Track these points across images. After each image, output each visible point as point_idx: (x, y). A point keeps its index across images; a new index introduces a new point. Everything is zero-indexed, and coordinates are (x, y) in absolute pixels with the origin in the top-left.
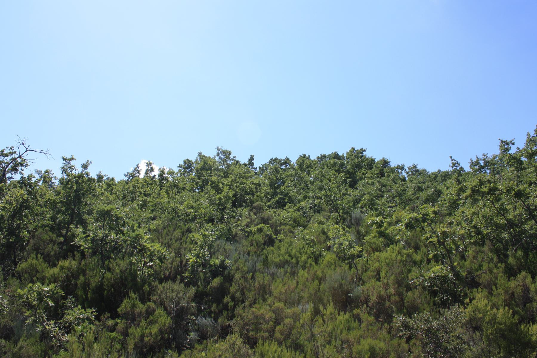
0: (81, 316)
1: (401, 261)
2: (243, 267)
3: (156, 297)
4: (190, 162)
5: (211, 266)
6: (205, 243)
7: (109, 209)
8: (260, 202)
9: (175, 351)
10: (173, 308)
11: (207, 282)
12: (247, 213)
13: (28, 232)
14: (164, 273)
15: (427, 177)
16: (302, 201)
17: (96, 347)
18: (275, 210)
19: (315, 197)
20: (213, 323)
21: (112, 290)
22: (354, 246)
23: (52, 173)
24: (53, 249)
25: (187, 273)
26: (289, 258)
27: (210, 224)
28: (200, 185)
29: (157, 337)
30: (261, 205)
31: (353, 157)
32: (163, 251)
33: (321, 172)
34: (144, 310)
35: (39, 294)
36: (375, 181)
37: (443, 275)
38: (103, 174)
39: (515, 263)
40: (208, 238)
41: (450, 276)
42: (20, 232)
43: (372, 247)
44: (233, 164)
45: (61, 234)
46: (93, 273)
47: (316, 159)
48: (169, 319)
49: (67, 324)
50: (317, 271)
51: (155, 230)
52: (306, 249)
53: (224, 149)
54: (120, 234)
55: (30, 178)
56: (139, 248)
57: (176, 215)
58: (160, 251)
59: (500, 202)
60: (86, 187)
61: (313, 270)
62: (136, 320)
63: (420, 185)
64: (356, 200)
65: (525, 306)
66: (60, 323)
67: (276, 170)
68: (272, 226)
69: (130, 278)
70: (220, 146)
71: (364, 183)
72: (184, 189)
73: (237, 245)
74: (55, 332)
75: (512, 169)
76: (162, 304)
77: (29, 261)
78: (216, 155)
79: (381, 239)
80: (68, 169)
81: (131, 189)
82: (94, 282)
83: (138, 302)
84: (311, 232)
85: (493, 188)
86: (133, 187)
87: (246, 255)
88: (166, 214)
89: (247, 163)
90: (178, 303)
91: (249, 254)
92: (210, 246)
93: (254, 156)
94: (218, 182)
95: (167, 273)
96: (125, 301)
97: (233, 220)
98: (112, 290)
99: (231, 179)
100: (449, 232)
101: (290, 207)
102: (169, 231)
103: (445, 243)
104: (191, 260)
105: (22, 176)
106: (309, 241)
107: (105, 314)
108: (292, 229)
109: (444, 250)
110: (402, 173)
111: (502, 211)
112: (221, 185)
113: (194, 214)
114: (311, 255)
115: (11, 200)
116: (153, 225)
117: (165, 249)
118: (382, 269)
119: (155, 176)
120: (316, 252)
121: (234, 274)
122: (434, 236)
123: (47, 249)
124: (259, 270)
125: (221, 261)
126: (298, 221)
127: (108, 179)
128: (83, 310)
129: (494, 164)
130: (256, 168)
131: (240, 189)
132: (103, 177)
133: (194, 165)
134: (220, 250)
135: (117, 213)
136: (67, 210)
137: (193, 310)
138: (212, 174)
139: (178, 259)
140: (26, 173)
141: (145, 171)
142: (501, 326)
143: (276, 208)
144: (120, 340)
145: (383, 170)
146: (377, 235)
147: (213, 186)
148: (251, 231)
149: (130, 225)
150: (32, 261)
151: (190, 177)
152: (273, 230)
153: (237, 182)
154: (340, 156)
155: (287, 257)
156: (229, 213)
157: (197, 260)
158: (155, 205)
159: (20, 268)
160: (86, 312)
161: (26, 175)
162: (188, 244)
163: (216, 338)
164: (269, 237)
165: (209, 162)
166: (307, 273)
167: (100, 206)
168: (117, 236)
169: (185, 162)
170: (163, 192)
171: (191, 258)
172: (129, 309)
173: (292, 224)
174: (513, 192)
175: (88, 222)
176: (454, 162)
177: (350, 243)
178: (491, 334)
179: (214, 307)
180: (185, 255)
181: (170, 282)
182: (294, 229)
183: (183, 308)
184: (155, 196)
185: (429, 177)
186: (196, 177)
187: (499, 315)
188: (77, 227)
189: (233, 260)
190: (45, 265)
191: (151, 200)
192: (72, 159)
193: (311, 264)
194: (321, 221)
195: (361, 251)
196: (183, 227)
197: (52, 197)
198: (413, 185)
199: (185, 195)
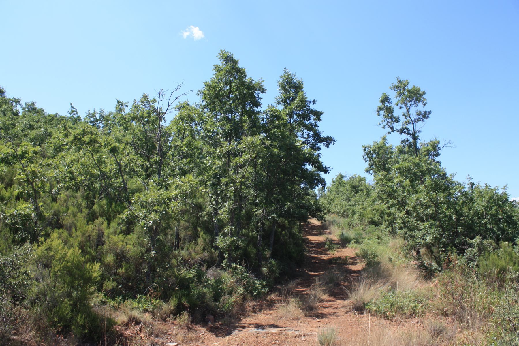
15: (44, 117)
37: (26, 213)
39: (98, 210)
41: (33, 215)
59: (99, 154)
63: (32, 123)
65: (97, 247)
75: (121, 128)
85: (93, 139)
100: (39, 172)
103: (34, 183)
109: (31, 189)
110: (16, 106)
111: (100, 163)
122: (23, 173)
129: (108, 120)
142: (69, 264)
174: (110, 147)
176: (73, 110)
178: (58, 270)
185: (45, 117)
187: (69, 255)
198: (25, 122)
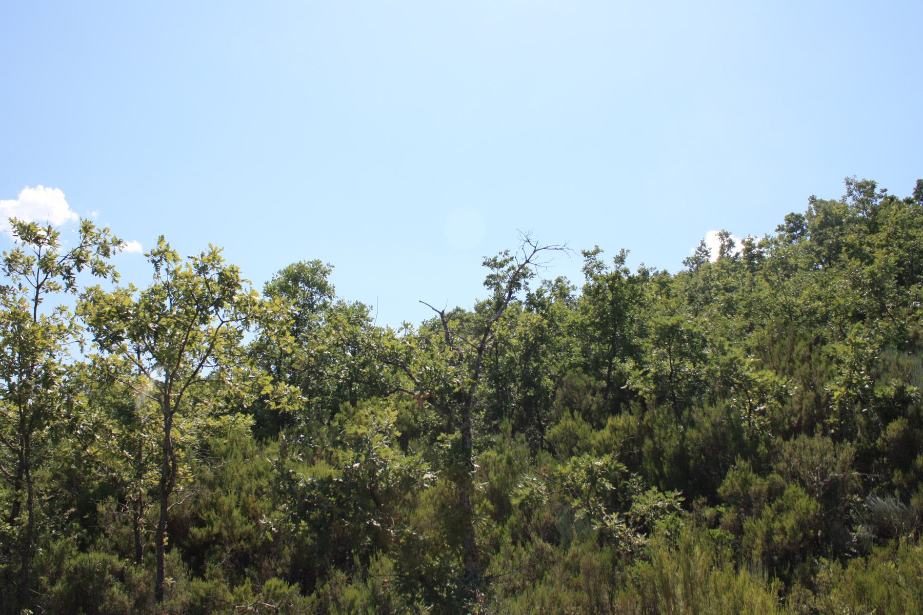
0: (659, 504)
3: (782, 465)
4: (798, 217)
5: (877, 400)
6: (859, 358)
7: (675, 322)
9: (834, 559)
10: (818, 482)
11: (873, 430)
13: (551, 377)
14: (790, 423)
17: (698, 554)
20: (902, 508)
21: (703, 457)
23: (567, 281)
24: (593, 401)
25: (831, 416)
28: (824, 256)
29: (796, 534)
32: (781, 382)
34: (765, 488)
35: (590, 471)
38: (647, 267)
40: (864, 348)
42: (539, 380)
45: (601, 375)
46: (667, 433)
48: (814, 501)
49: (639, 518)
51: (757, 348)
54: (699, 362)
55: (540, 293)
56: (738, 381)
57: (790, 316)
58: (777, 383)
60: (627, 294)
62: (752, 507)
66: (627, 517)
69: (731, 436)
70: (851, 176)
74: (621, 531)
76: (794, 476)
77: (562, 422)
78: (846, 194)
80: (595, 269)
81: (701, 284)
82: (670, 446)
83: (751, 475)
86: (704, 280)
88: (772, 317)
89: (912, 197)
90: (824, 475)
92: (871, 364)
94: (861, 244)
95: (795, 420)
96: (729, 475)
98: (703, 457)
99: (885, 234)
102: (782, 346)
104: (836, 394)
105: (528, 292)
107: (698, 498)
112: (868, 249)
113: (824, 309)
115: (526, 331)
116: (752, 340)
117: (785, 378)
119: (738, 254)
123: (584, 402)
127: (656, 274)
128: (661, 494)
131: (908, 250)
132: (648, 273)
133: (806, 221)
135: (691, 327)
136: (604, 334)
137: (855, 485)
138: (844, 232)
139: (811, 394)
140: (534, 285)
141: (719, 249)
144: (729, 541)
149: (717, 345)
150: (567, 422)
153: (899, 238)
156: (894, 297)
157: (847, 393)
158: (750, 305)
159: (551, 434)
160: (667, 498)
161: (533, 291)
163: (911, 535)
165: (835, 211)
167: (658, 319)
168: (695, 366)
169: (788, 220)
170: (758, 278)
171: (835, 389)
172: (739, 488)
175: (644, 349)
179: (897, 476)
181: (803, 436)
183: (835, 483)
184: (746, 290)
186: (815, 243)
188: (623, 361)
190: (586, 426)
191: (740, 297)
192: (597, 251)
196: (808, 335)
197: (578, 318)
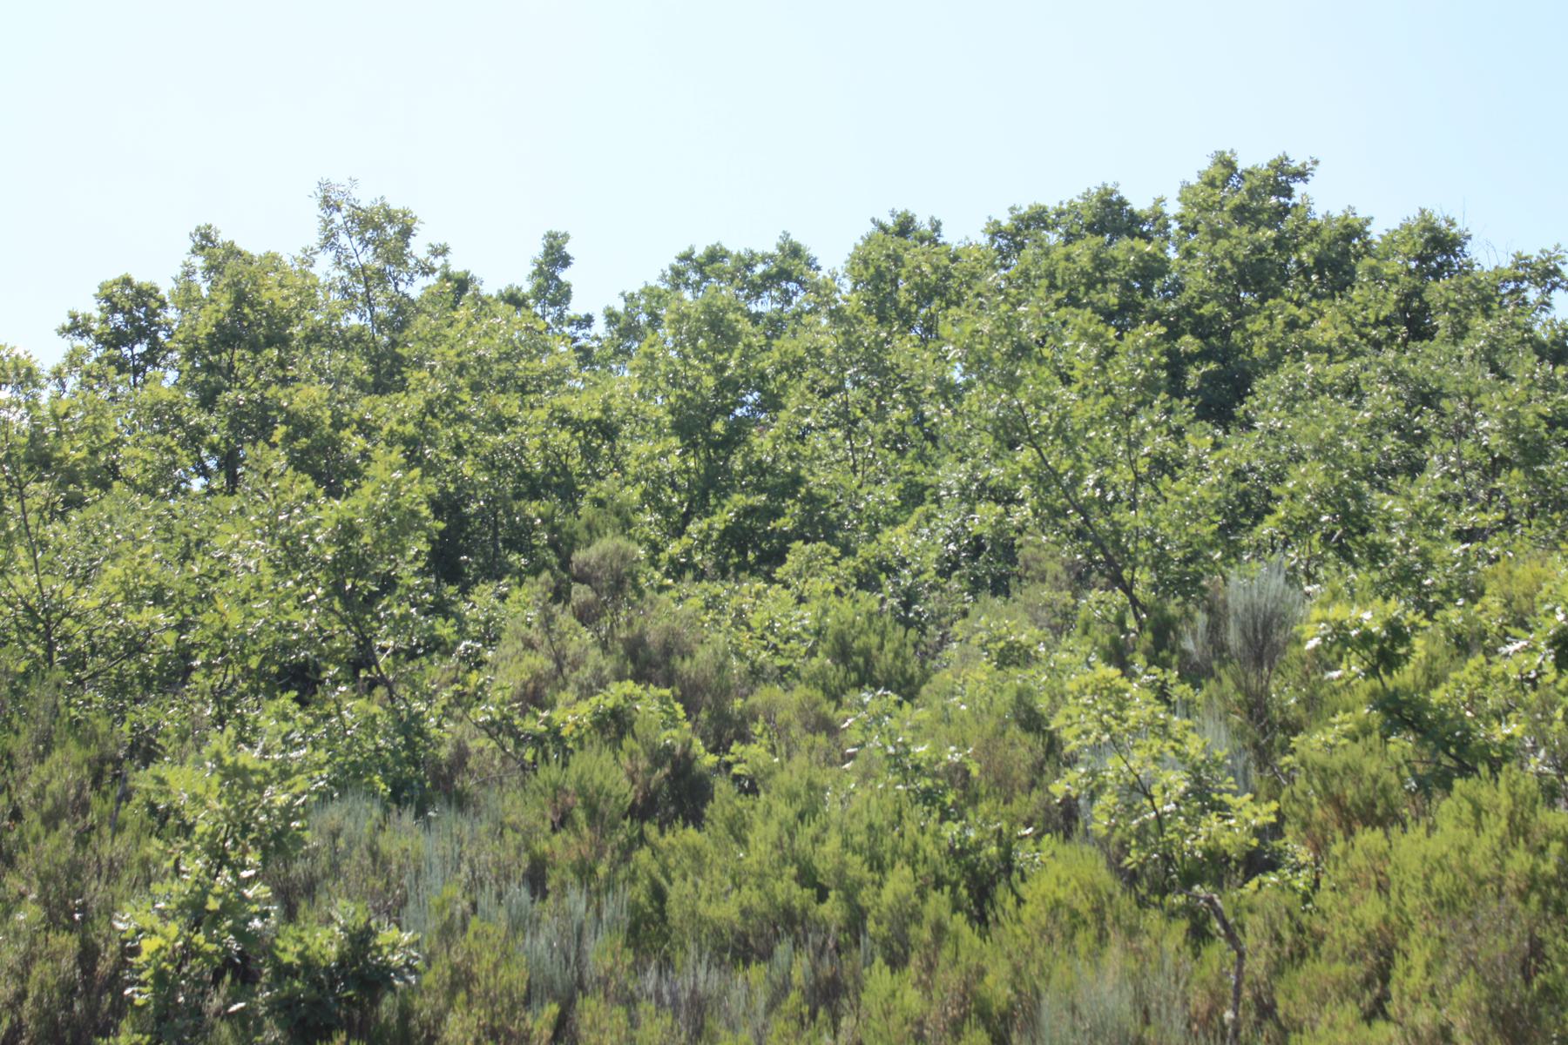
1: (1533, 881)
2: (496, 966)
4: (144, 295)
5: (283, 972)
8: (621, 541)
12: (533, 614)
16: (893, 522)
18: (718, 588)
19: (969, 497)
22: (1227, 798)
26: (800, 896)
27: (286, 701)
28: (214, 449)
30: (624, 558)
31: (1220, 219)
33: (1011, 323)
36: (1370, 368)
40: (260, 788)
43: (1336, 801)
44: (434, 297)
47: (984, 240)
50: (981, 973)
52: (910, 828)
53: (366, 199)
61: (955, 962)
64: (1243, 496)
67: (718, 328)
68: (691, 696)
70: (338, 178)
71: (1297, 386)
72: (106, 476)
73: (462, 826)
79: (1402, 744)
84: (949, 721)
87: (519, 893)
89: (527, 288)
91: (536, 879)
92: (278, 845)
93: (566, 236)
94: (338, 425)
97: (436, 670)
101: (809, 569)
104: (149, 945)
106: (935, 775)
108: (828, 708)
112: (359, 442)
113: (170, 637)
114: (945, 871)
118: (1405, 937)
120: (978, 846)
121: (440, 1018)
124: (603, 982)
125: (351, 938)
126: (866, 653)
130: (588, 321)
131: (489, 465)
133: (172, 314)
134: (349, 866)
138: (292, 371)
139: (68, 942)
143: (722, 571)
145: (1417, 293)
146: (1376, 718)
147: (306, 452)
148: (556, 734)
151: (144, 395)
152: (704, 715)
154: (1135, 219)
155: (787, 889)
156: (405, 617)
162: (128, 835)
164: (675, 765)
166: (919, 983)
173: (822, 672)
177: (1199, 780)
180: (110, 911)
182: (839, 705)
189: (434, 924)
193: (939, 929)
194: (1011, 647)
195: (1276, 830)
196: (102, 725)
199: (110, 520)
